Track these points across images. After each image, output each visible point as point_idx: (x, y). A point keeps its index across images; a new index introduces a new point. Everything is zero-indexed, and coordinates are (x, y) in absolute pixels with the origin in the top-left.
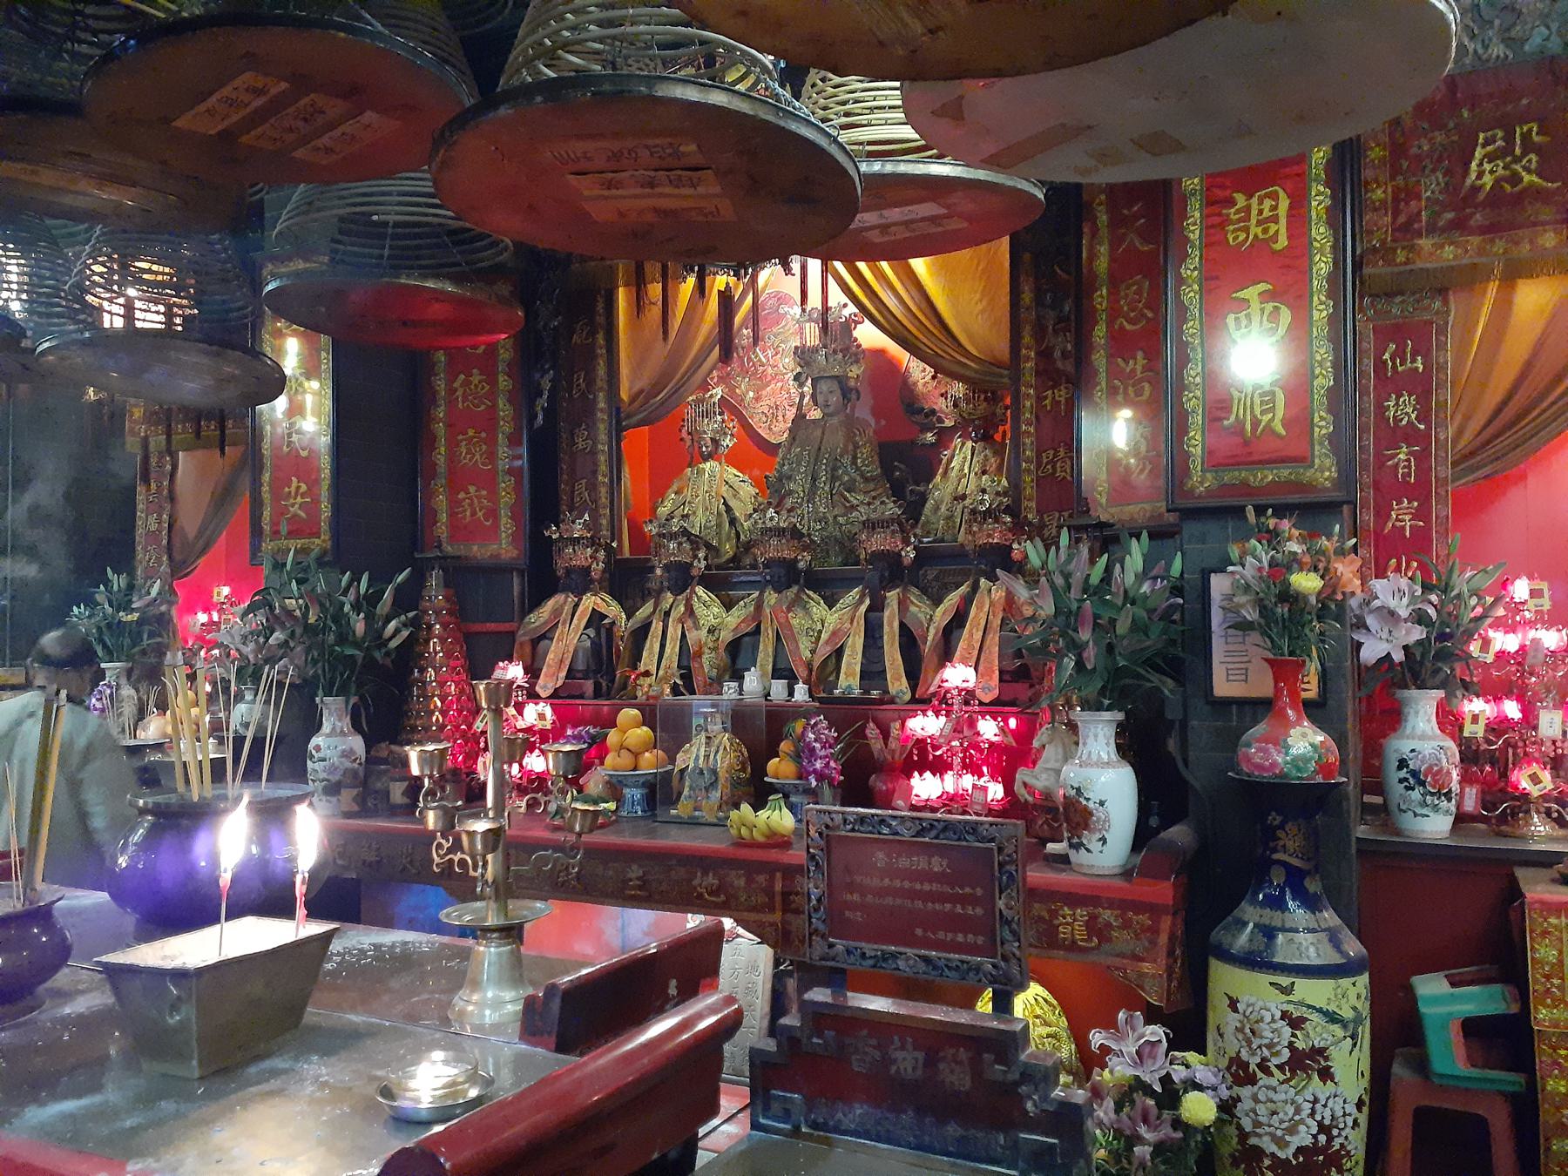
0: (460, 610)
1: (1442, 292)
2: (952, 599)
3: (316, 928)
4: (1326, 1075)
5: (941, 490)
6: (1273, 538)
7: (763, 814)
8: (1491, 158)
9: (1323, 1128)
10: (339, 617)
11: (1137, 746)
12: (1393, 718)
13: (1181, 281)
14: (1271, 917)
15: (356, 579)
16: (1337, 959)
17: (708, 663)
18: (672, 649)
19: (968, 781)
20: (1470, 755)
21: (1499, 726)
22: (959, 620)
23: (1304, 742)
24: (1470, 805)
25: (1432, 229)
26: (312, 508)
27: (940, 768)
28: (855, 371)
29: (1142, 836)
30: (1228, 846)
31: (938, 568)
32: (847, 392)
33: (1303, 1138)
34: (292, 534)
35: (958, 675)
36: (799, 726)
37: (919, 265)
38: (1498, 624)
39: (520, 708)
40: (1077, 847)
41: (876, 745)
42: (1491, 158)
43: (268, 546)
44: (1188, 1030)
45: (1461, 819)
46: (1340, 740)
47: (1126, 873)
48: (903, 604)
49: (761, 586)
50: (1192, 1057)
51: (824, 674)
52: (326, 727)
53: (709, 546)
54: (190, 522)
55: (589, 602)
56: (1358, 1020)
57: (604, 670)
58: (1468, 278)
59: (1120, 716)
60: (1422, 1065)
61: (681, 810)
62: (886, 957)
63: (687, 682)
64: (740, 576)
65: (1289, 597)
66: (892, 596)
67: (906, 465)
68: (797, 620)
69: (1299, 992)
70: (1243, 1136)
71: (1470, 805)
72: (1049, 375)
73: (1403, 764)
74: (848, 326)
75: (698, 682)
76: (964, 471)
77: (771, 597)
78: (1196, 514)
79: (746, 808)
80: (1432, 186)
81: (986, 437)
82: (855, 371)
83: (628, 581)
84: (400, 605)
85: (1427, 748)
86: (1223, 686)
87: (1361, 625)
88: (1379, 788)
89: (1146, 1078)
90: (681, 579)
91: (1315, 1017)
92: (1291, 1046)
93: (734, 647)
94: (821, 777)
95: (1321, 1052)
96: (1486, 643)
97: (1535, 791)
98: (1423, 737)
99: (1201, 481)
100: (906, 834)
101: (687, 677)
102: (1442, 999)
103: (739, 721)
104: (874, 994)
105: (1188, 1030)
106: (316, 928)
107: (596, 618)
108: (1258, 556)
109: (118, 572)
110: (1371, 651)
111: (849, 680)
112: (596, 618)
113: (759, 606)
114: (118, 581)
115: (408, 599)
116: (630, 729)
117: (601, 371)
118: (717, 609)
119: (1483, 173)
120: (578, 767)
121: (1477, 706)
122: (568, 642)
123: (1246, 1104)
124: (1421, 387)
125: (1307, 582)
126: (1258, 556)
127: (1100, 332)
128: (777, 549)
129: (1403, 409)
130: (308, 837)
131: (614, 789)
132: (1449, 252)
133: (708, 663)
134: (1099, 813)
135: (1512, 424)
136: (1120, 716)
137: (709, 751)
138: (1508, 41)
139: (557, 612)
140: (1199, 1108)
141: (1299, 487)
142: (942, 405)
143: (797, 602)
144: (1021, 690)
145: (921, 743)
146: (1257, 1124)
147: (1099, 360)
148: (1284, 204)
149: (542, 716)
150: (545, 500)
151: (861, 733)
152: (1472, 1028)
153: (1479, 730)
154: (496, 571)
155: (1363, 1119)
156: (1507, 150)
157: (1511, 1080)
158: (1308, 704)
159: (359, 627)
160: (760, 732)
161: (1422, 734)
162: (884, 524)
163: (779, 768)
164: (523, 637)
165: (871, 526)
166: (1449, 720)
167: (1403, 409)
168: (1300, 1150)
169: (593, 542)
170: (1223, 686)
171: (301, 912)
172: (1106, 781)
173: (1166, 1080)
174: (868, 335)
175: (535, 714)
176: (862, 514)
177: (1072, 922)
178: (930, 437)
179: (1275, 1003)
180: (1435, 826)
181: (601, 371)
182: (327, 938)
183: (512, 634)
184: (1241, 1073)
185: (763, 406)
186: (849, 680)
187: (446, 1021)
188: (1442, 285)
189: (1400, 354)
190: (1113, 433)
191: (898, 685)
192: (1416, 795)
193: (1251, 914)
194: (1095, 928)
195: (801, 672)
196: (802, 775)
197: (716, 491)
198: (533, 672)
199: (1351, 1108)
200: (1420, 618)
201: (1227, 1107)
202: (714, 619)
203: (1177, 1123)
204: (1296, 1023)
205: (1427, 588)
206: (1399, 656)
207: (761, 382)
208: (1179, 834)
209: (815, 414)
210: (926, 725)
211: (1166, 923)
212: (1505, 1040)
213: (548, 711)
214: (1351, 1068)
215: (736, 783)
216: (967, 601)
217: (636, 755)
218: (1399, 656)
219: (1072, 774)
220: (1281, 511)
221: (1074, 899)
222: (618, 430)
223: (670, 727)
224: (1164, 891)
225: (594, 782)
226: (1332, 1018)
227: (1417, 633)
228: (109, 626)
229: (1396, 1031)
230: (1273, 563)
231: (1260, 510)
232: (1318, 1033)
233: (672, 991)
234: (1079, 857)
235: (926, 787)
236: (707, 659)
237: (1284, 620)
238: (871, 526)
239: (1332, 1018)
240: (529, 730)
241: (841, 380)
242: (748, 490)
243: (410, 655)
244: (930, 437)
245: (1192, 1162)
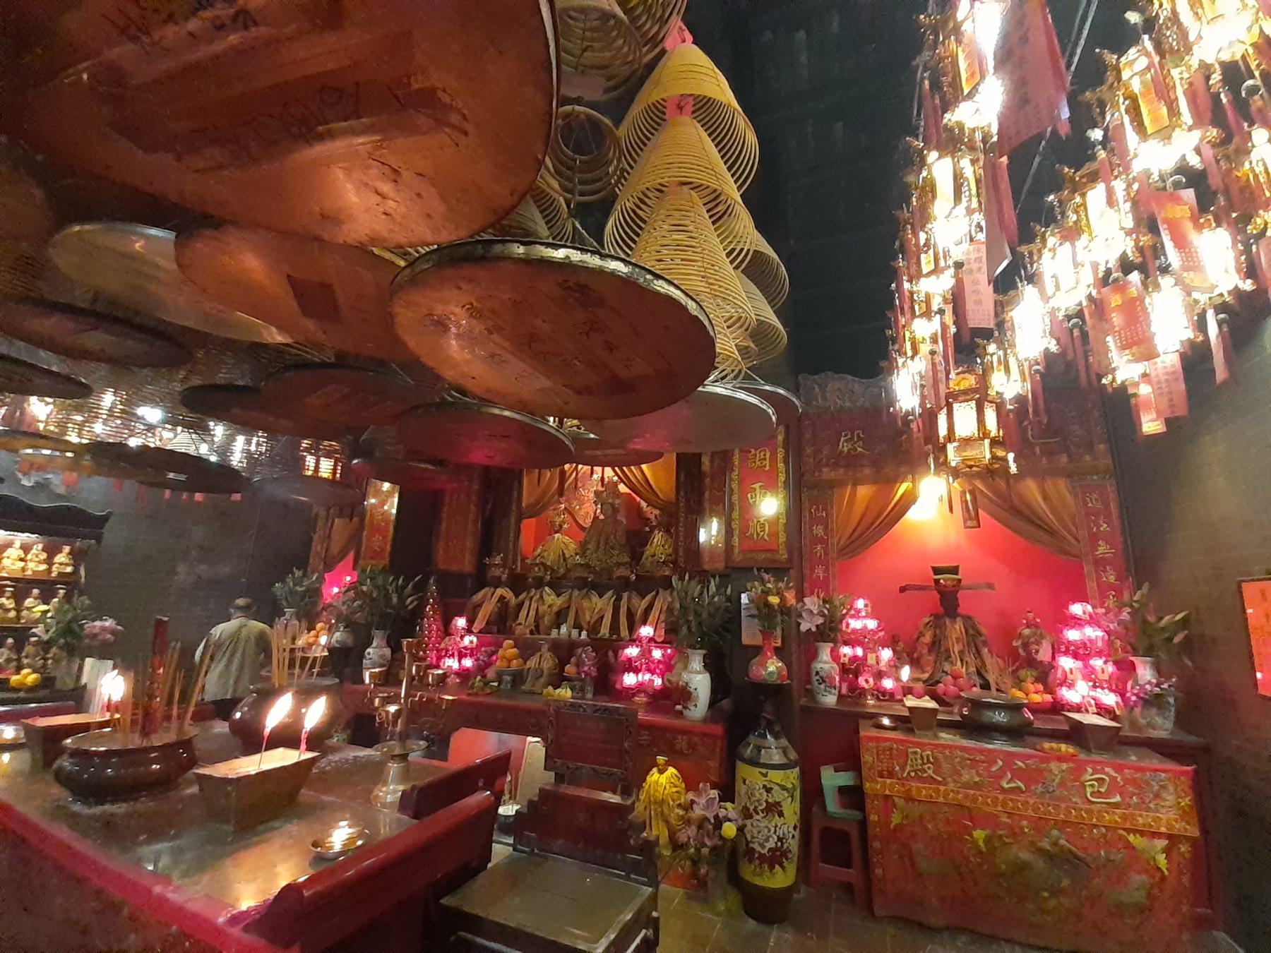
0: (443, 592)
1: (832, 488)
2: (649, 597)
3: (310, 755)
4: (781, 814)
5: (649, 550)
6: (763, 582)
7: (558, 691)
8: (846, 441)
9: (780, 839)
10: (387, 596)
11: (713, 665)
12: (813, 655)
13: (731, 480)
14: (759, 742)
15: (397, 579)
16: (784, 761)
17: (547, 620)
18: (532, 613)
19: (648, 676)
20: (844, 670)
21: (855, 658)
22: (650, 607)
23: (773, 667)
24: (844, 691)
25: (827, 465)
26: (383, 550)
27: (637, 671)
28: (617, 502)
29: (713, 703)
30: (747, 710)
31: (647, 584)
32: (615, 510)
33: (771, 844)
34: (372, 558)
35: (646, 631)
36: (580, 650)
37: (644, 466)
38: (852, 617)
39: (462, 637)
40: (685, 708)
41: (612, 659)
42: (846, 441)
43: (361, 562)
44: (728, 794)
45: (840, 697)
46: (788, 665)
47: (705, 720)
48: (629, 599)
49: (573, 588)
50: (728, 805)
51: (594, 629)
52: (374, 644)
53: (553, 570)
54: (335, 549)
55: (500, 591)
56: (794, 788)
57: (502, 623)
58: (842, 484)
59: (704, 652)
60: (824, 806)
61: (526, 687)
62: (577, 768)
63: (537, 629)
64: (564, 582)
65: (768, 605)
66: (625, 595)
67: (636, 540)
68: (585, 604)
69: (771, 775)
70: (748, 843)
71: (844, 691)
72: (690, 510)
73: (817, 673)
74: (616, 484)
75: (541, 629)
76: (658, 544)
77: (576, 593)
78: (735, 570)
79: (550, 688)
80: (826, 450)
81: (668, 531)
82: (617, 502)
83: (518, 583)
84: (416, 589)
85: (826, 666)
86: (746, 640)
87: (800, 616)
88: (809, 681)
89: (708, 815)
90: (539, 584)
91: (776, 788)
92: (767, 801)
93: (558, 614)
94: (586, 674)
95: (778, 804)
96: (848, 625)
97: (866, 686)
98: (825, 662)
99: (737, 556)
100: (589, 711)
101: (537, 627)
102: (832, 779)
103: (556, 646)
104: (398, 836)
105: (728, 794)
106: (310, 755)
107: (502, 598)
108: (758, 587)
109: (298, 569)
110: (804, 627)
111: (604, 631)
112: (502, 598)
113: (571, 596)
114: (298, 573)
115: (421, 588)
116: (509, 649)
117: (515, 494)
118: (553, 597)
119: (844, 447)
120: (481, 669)
121: (846, 650)
122: (488, 608)
123: (749, 827)
124: (825, 523)
125: (774, 600)
126: (758, 587)
127: (707, 494)
128: (579, 573)
129: (819, 530)
130: (316, 713)
131: (499, 677)
132: (833, 474)
133: (547, 620)
134: (694, 694)
135: (860, 536)
136: (704, 652)
137: (545, 661)
138: (850, 401)
139: (485, 595)
140: (729, 830)
141: (775, 561)
142: (652, 517)
143: (587, 596)
144: (672, 636)
145: (630, 660)
146: (753, 837)
147: (707, 505)
148: (768, 455)
149: (471, 642)
150: (486, 546)
151: (606, 654)
152: (842, 790)
153: (846, 660)
154: (461, 576)
155: (797, 834)
156: (852, 439)
157: (855, 814)
158: (776, 649)
159: (395, 600)
160: (564, 652)
161: (825, 662)
162: (623, 564)
163: (570, 669)
164: (469, 606)
165: (619, 565)
166: (835, 656)
167: (819, 530)
168: (770, 850)
169: (504, 566)
170: (746, 640)
171: (303, 746)
172: (699, 682)
173: (716, 817)
174: (623, 488)
175: (468, 640)
176: (615, 560)
177: (682, 742)
178: (647, 529)
179: (761, 781)
180: (830, 700)
181: (515, 494)
182: (314, 760)
183: (465, 605)
184: (747, 814)
185: (582, 512)
186: (604, 631)
187: (369, 800)
188: (831, 485)
189: (817, 509)
190: (710, 532)
191: (624, 633)
192: (822, 686)
193: (753, 740)
194: (692, 746)
195: (585, 626)
196: (579, 673)
197: (563, 544)
198: (471, 622)
199: (791, 829)
200: (821, 614)
201: (741, 829)
202: (552, 599)
203: (721, 838)
204: (769, 790)
205: (825, 602)
206: (814, 629)
207: (582, 504)
208: (726, 703)
209: (602, 517)
210: (632, 651)
211: (719, 742)
212: (853, 796)
213: (475, 639)
214: (792, 809)
215: (551, 675)
216: (654, 598)
217: (509, 661)
218: (814, 629)
219: (685, 676)
220: (767, 571)
221: (684, 732)
222: (519, 521)
223: (527, 649)
224: (718, 729)
225: (491, 673)
226: (784, 788)
227: (821, 621)
228: (291, 593)
229: (811, 792)
230: (763, 592)
231: (759, 570)
232: (778, 795)
233: (480, 784)
234: (686, 712)
235: (630, 679)
236: (546, 619)
237: (765, 612)
238: (619, 565)
239: (784, 788)
240: (465, 648)
241: (612, 505)
242: (572, 546)
243: (418, 613)
244: (647, 529)
245: (726, 855)
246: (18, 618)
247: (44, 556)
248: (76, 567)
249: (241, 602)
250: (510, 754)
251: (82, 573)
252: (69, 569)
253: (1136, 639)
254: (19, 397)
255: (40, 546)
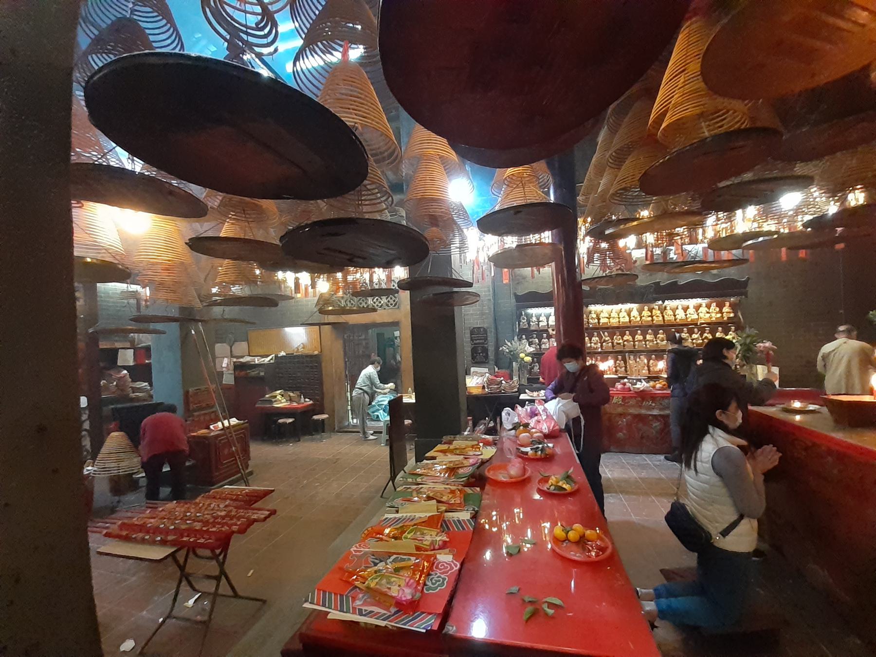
246: (630, 322)
247: (718, 309)
248: (735, 312)
249: (842, 328)
250: (661, 571)
251: (740, 314)
252: (732, 315)
253: (768, 383)
254: (77, 270)
255: (714, 304)
